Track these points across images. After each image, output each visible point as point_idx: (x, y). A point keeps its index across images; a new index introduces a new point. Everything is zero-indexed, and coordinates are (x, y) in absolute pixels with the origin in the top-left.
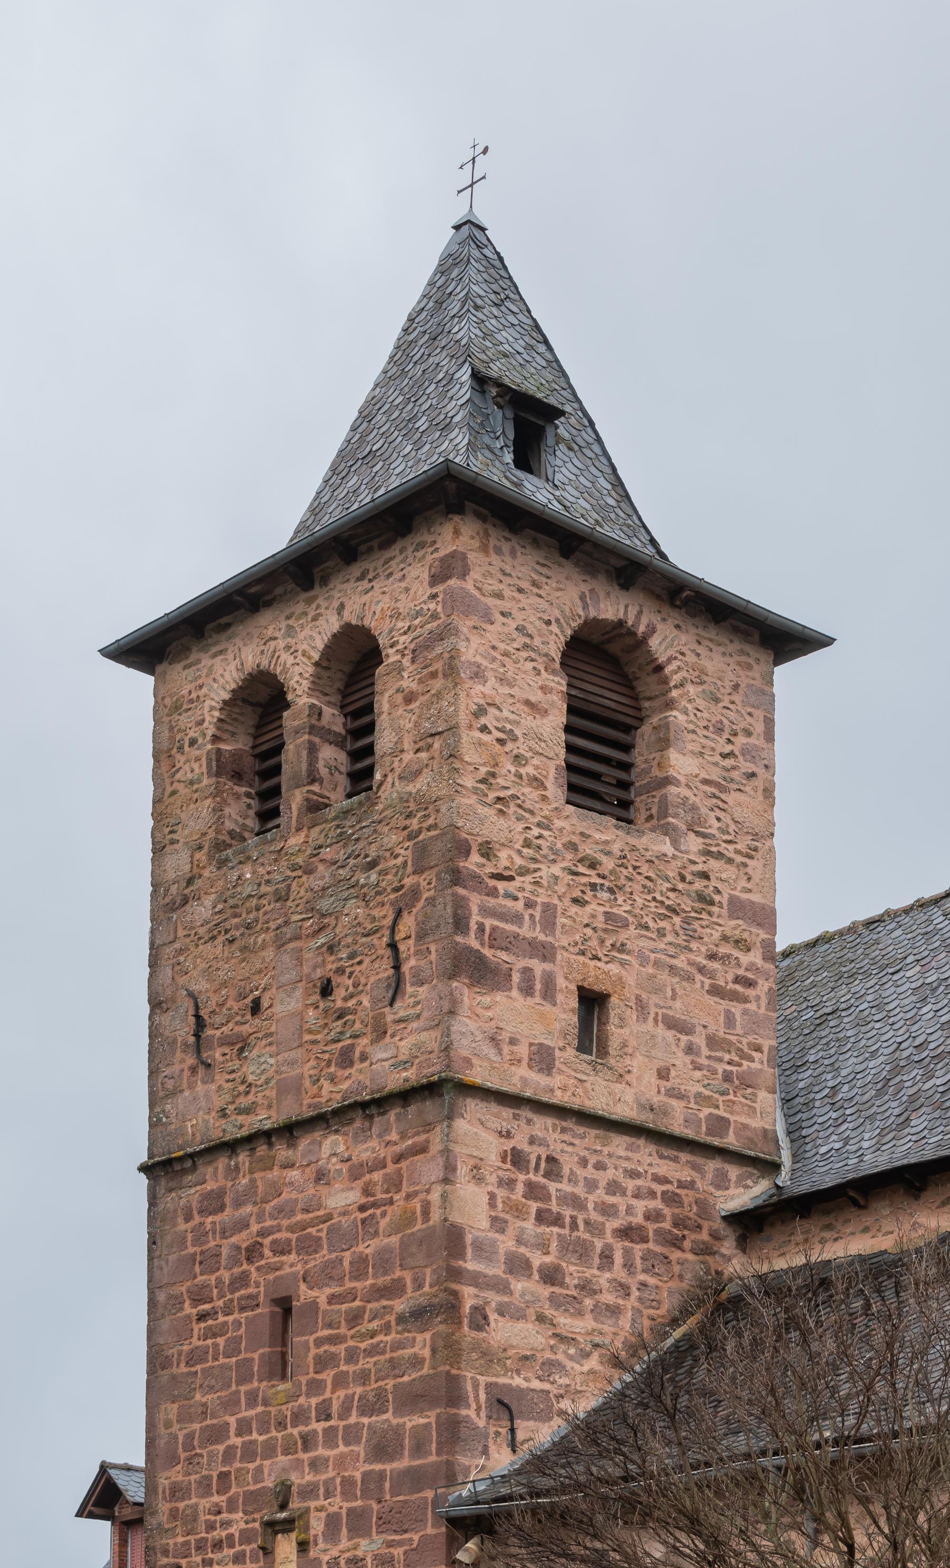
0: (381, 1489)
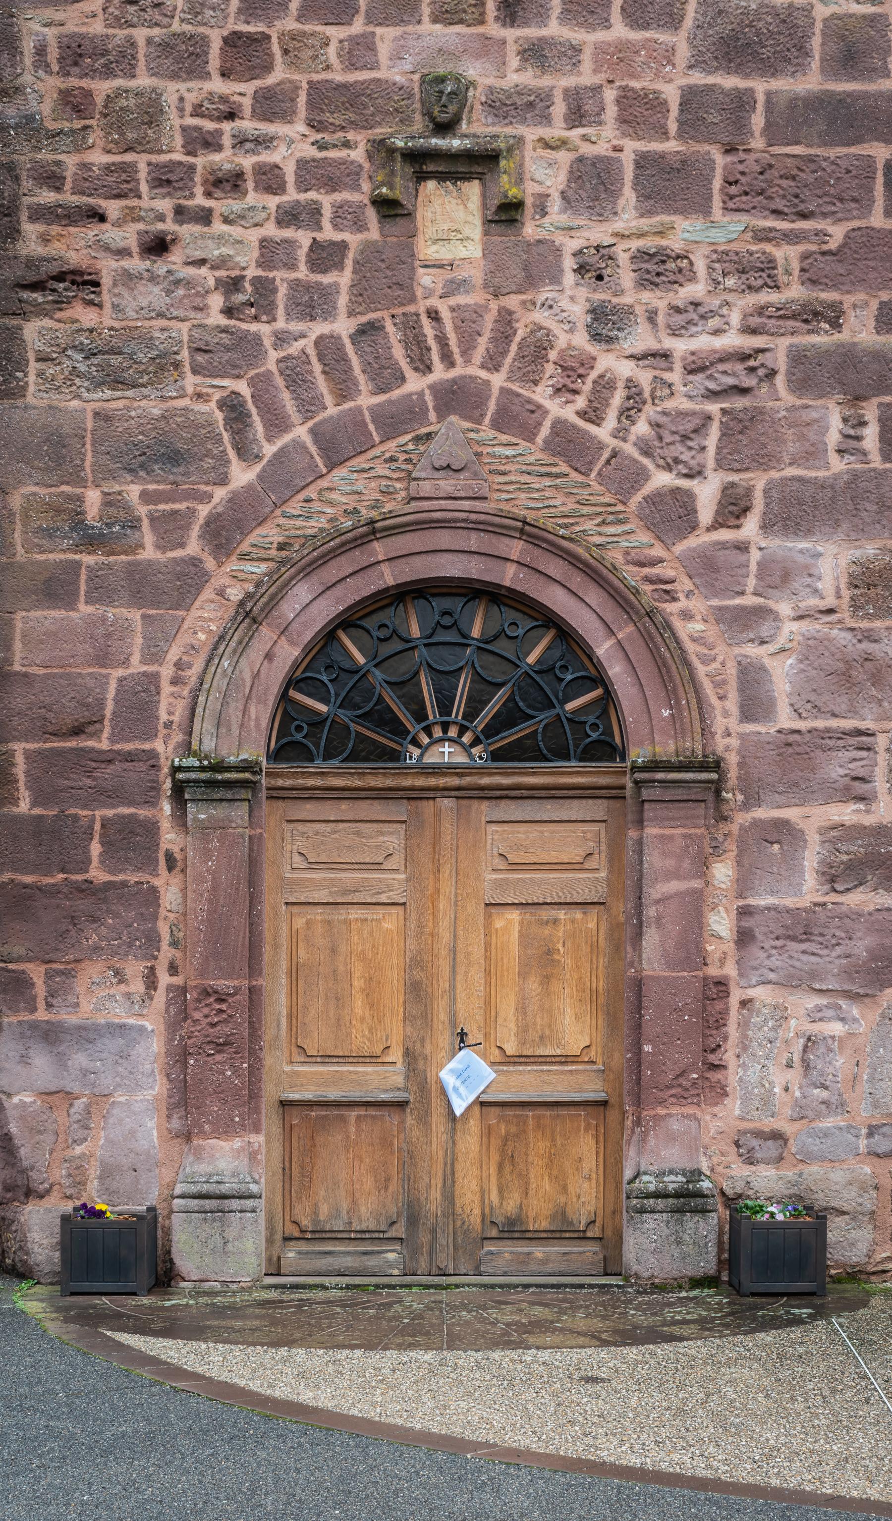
0: (741, 126)
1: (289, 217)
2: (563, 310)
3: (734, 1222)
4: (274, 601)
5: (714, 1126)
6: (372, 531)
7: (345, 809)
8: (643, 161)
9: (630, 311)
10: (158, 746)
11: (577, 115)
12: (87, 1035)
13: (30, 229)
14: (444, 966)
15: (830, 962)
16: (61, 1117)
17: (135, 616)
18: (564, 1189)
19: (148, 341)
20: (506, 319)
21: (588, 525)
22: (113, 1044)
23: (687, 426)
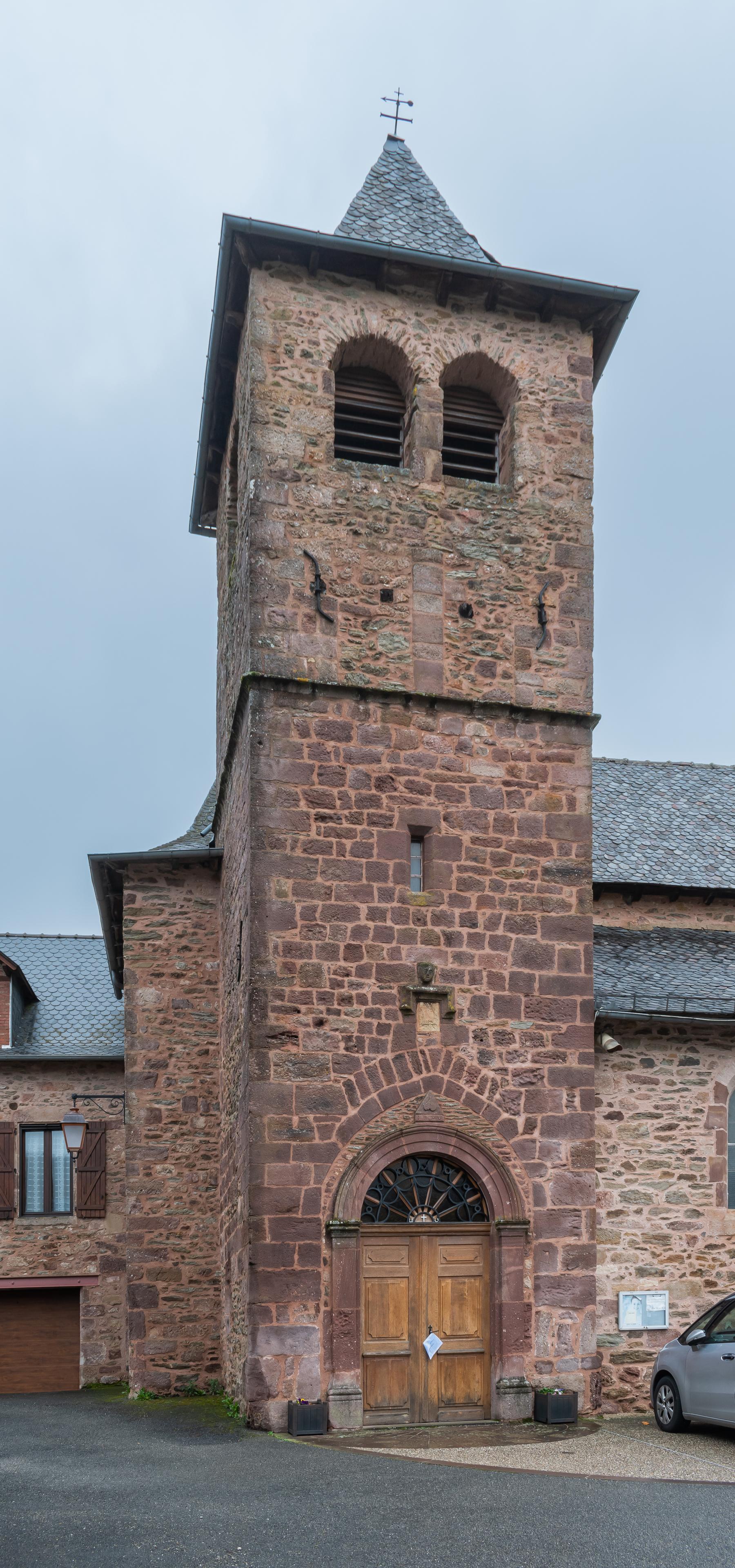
0: (531, 988)
1: (369, 1014)
2: (470, 1051)
3: (536, 1395)
4: (366, 1159)
5: (527, 1360)
6: (402, 1133)
7: (386, 1240)
8: (497, 998)
9: (493, 1053)
10: (321, 1217)
11: (474, 980)
12: (293, 1331)
13: (272, 1015)
14: (424, 1300)
15: (567, 1296)
16: (282, 1365)
17: (312, 1165)
18: (469, 1387)
19: (317, 1059)
20: (449, 1055)
21: (479, 1132)
22: (302, 1335)
23: (514, 1096)
